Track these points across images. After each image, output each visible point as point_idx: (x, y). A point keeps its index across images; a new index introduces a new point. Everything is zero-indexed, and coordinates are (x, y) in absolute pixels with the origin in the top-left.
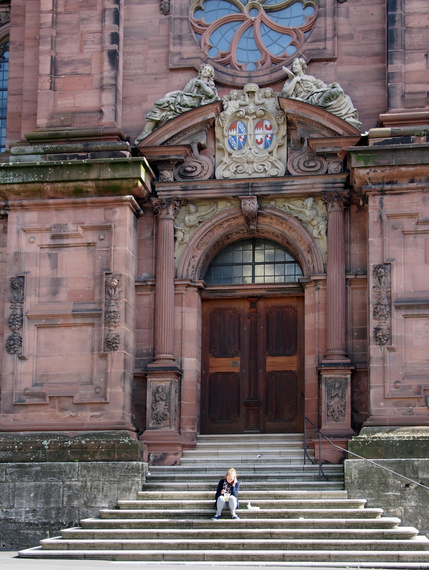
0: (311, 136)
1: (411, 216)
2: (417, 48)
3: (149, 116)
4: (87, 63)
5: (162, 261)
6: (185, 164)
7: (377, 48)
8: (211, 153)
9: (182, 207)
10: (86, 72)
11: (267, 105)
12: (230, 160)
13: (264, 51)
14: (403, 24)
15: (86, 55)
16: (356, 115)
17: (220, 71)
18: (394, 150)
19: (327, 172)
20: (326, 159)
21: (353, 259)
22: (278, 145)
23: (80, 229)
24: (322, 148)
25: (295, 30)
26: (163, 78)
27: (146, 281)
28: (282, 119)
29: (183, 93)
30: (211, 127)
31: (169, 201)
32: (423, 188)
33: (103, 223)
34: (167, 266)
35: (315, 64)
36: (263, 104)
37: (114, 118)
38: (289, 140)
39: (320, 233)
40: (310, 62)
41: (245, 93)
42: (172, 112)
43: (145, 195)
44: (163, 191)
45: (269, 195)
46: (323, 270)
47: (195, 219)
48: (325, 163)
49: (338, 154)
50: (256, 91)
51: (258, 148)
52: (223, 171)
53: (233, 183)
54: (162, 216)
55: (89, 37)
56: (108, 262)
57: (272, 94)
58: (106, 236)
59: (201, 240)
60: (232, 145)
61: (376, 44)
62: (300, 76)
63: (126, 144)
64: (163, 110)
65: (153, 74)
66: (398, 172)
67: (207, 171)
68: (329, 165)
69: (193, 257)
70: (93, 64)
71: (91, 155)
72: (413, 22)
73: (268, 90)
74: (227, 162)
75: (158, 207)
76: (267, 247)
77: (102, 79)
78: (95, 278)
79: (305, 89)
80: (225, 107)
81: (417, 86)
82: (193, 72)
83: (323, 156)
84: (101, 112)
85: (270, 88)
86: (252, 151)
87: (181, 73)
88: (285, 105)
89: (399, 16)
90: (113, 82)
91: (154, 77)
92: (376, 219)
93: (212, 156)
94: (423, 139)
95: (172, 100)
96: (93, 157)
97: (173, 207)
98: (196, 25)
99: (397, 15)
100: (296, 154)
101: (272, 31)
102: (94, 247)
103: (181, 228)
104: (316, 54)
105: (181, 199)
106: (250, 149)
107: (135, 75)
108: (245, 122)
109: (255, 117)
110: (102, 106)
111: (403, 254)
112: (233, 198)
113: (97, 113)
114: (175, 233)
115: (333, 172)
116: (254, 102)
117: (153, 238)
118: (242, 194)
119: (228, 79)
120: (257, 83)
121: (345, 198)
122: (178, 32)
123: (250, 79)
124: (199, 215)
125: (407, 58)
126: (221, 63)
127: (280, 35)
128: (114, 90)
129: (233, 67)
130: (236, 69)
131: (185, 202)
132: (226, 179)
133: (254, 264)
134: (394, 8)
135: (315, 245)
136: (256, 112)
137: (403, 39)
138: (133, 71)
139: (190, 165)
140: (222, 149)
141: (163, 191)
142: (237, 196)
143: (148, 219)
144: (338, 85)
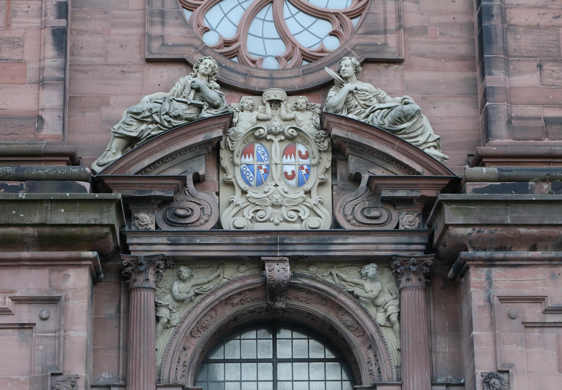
0: (370, 171)
3: (118, 129)
4: (18, 43)
5: (138, 355)
6: (175, 204)
7: (463, 49)
8: (213, 188)
9: (168, 270)
10: (15, 57)
11: (300, 121)
15: (15, 33)
16: (438, 145)
17: (225, 67)
18: (507, 202)
19: (397, 227)
20: (395, 207)
21: (440, 360)
23: (8, 300)
25: (337, 14)
26: (134, 72)
28: (326, 144)
30: (213, 149)
31: (150, 260)
32: (551, 259)
35: (371, 66)
36: (294, 119)
38: (334, 175)
39: (388, 319)
41: (265, 102)
43: (111, 249)
45: (307, 256)
46: (395, 376)
47: (188, 290)
48: (395, 214)
49: (415, 201)
50: (283, 100)
51: (289, 185)
52: (233, 217)
53: (250, 239)
54: (136, 284)
55: (20, 6)
57: (308, 105)
58: (52, 313)
59: (198, 323)
60: (248, 178)
61: (460, 44)
62: (352, 82)
63: (85, 171)
64: (141, 121)
65: (118, 65)
67: (209, 216)
68: (401, 217)
69: (185, 349)
70: (26, 46)
73: (302, 100)
75: (131, 270)
76: (296, 335)
79: (362, 102)
80: (235, 120)
81: (528, 108)
84: (40, 119)
85: (304, 97)
87: (163, 66)
90: (59, 75)
91: (120, 69)
92: (482, 303)
95: (156, 107)
97: (154, 269)
99: (495, 7)
100: (349, 197)
101: (301, 13)
102: (30, 330)
103: (167, 303)
104: (372, 52)
107: (90, 65)
108: (267, 145)
110: (42, 109)
115: (407, 227)
116: (280, 116)
118: (266, 254)
119: (238, 81)
120: (283, 88)
124: (195, 284)
125: (511, 67)
126: (225, 55)
127: (315, 19)
128: (62, 86)
130: (248, 65)
131: (173, 263)
132: (239, 232)
133: (275, 361)
135: (382, 337)
136: (283, 131)
137: (505, 41)
138: (87, 59)
140: (230, 184)
143: (110, 287)
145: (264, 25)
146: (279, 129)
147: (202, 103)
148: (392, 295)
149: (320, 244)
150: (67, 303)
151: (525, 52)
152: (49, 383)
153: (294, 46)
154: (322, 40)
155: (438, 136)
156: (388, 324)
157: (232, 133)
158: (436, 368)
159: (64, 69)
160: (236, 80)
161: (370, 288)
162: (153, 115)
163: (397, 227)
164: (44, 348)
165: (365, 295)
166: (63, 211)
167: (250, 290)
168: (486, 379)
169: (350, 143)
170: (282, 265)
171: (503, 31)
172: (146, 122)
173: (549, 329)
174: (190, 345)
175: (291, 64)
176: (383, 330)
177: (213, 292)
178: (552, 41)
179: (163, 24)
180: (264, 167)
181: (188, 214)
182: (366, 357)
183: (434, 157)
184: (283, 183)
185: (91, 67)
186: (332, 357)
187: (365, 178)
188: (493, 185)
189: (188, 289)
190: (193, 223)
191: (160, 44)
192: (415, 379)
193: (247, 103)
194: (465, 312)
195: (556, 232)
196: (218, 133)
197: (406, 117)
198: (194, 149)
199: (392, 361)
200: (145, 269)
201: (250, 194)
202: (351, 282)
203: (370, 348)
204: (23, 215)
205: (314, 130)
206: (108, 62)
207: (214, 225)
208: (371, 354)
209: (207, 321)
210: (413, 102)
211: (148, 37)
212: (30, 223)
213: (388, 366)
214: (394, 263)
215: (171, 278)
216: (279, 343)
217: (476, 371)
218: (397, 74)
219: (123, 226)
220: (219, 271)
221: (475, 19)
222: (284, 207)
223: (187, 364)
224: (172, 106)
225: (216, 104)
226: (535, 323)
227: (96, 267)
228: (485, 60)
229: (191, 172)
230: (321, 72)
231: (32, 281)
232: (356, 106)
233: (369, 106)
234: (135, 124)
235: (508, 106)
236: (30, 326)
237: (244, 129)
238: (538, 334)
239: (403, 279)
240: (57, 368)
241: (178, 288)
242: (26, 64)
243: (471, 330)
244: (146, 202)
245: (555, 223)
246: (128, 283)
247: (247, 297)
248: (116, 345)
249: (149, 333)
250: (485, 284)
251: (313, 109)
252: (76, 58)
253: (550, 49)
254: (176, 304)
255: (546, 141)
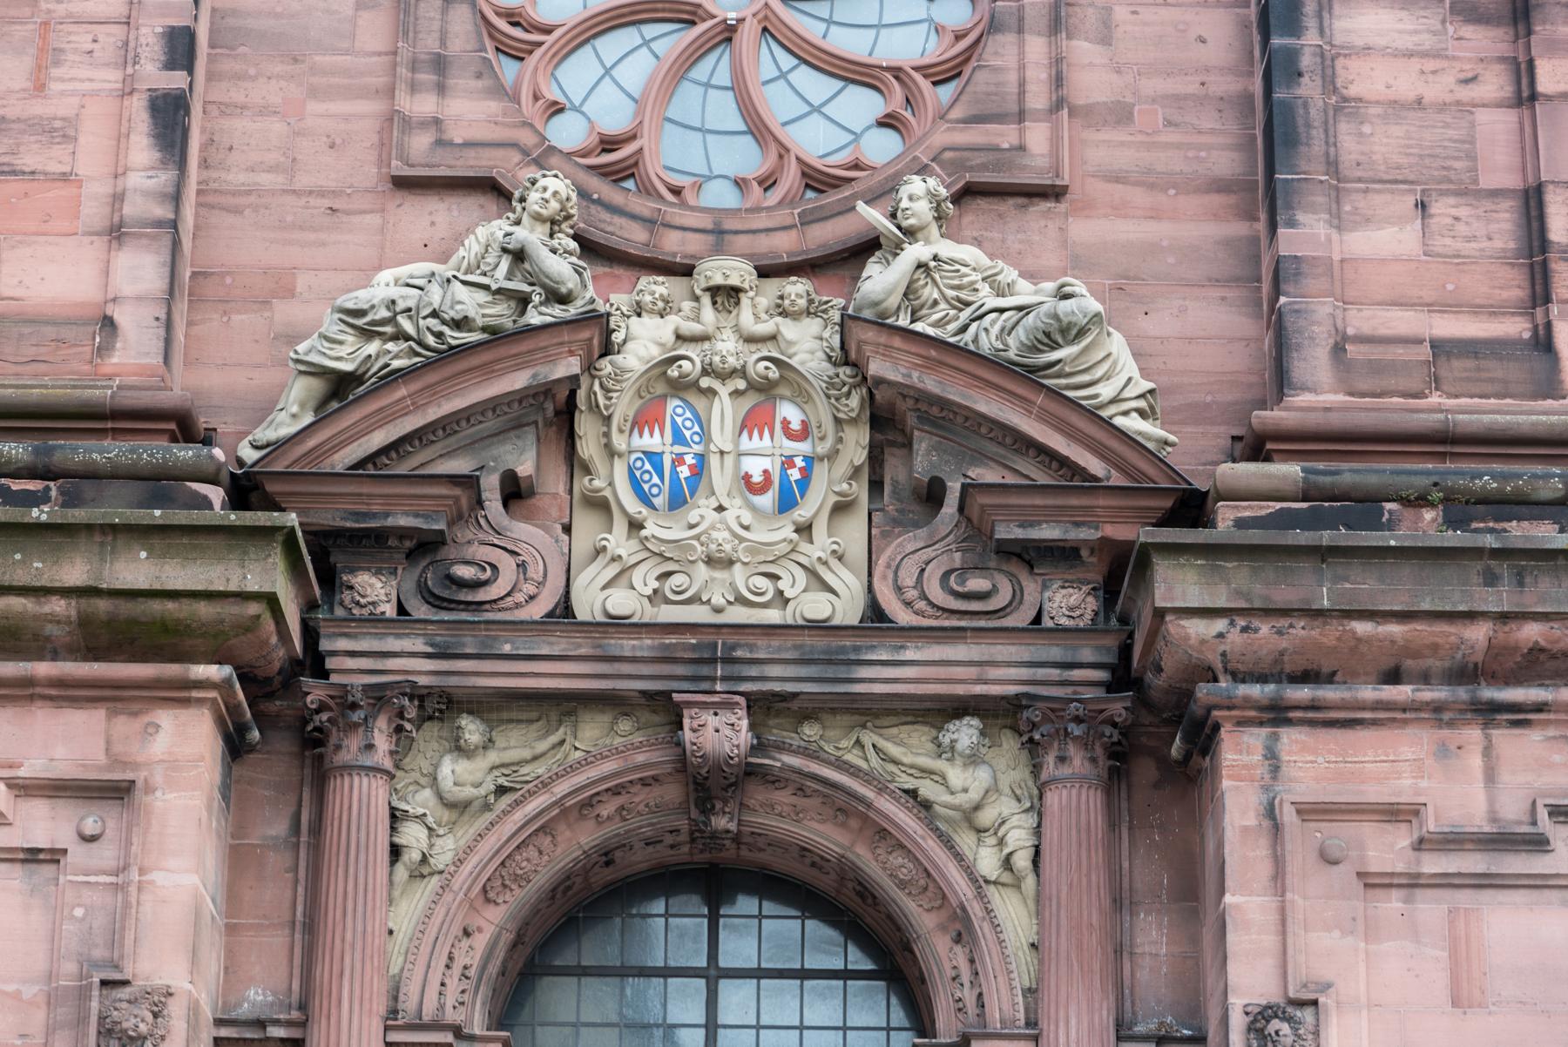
0: (970, 473)
1: (1395, 813)
2: (1386, 177)
3: (306, 354)
4: (61, 132)
6: (449, 552)
7: (1225, 162)
8: (554, 512)
9: (427, 724)
11: (790, 343)
12: (634, 545)
13: (776, 139)
14: (1330, 83)
15: (56, 106)
16: (1152, 407)
17: (599, 202)
19: (1037, 620)
20: (1032, 567)
21: (1143, 975)
22: (834, 499)
24: (1021, 526)
25: (897, 72)
27: (261, 1024)
28: (854, 401)
29: (449, 274)
30: (557, 413)
31: (379, 696)
32: (1437, 708)
33: (100, 769)
34: (358, 965)
35: (982, 203)
37: (162, 351)
38: (876, 486)
39: (1007, 864)
40: (967, 194)
41: (698, 292)
42: (404, 345)
43: (277, 665)
44: (352, 654)
45: (795, 695)
46: (1021, 1016)
48: (1031, 587)
49: (1084, 553)
51: (753, 509)
52: (604, 588)
53: (644, 645)
54: (344, 757)
55: (72, 38)
56: (115, 936)
57: (811, 302)
58: (111, 824)
59: (503, 863)
60: (646, 487)
61: (1220, 151)
62: (927, 242)
63: (212, 457)
64: (367, 334)
65: (322, 193)
66: (1339, 639)
67: (541, 584)
68: (1047, 594)
69: (467, 933)
70: (82, 140)
71: (62, 492)
72: (1366, 80)
73: (797, 288)
74: (622, 552)
75: (329, 720)
76: (769, 907)
77: (118, 198)
78: (52, 999)
79: (951, 293)
80: (618, 337)
81: (1389, 314)
82: (489, 196)
83: (1019, 556)
84: (108, 323)
86: (723, 516)
88: (868, 350)
89: (1314, 55)
90: (163, 212)
91: (327, 203)
92: (1251, 820)
93: (559, 528)
94: (1428, 515)
95: (409, 298)
96: (70, 500)
97: (390, 721)
98: (502, 24)
99: (1307, 50)
100: (910, 541)
101: (804, 67)
102: (53, 867)
103: (421, 811)
104: (984, 167)
105: (425, 691)
106: (720, 509)
107: (249, 193)
108: (700, 403)
109: (741, 384)
110: (114, 300)
111: (1362, 968)
112: (643, 701)
113: (90, 329)
114: (393, 829)
115: (1064, 621)
117: (297, 846)
119: (632, 236)
121: (1115, 725)
122: (430, 43)
123: (720, 236)
124: (498, 762)
125: (1347, 208)
126: (603, 171)
127: (841, 84)
128: (166, 241)
129: (647, 190)
130: (661, 197)
131: (440, 706)
132: (617, 624)
133: (713, 974)
134: (1294, 27)
135: (989, 911)
137: (1332, 140)
139: (469, 557)
140: (601, 505)
141: (352, 654)
142: (667, 695)
143: (276, 763)
144: (1079, 287)
145: (708, 100)
146: (732, 361)
147: (527, 289)
148: (1019, 800)
149: (830, 662)
150: (148, 799)
151: (1382, 168)
152: (95, 1005)
153: (784, 151)
154: (857, 137)
155: (1150, 385)
156: (1006, 878)
157: (609, 369)
158: (1132, 994)
159: (176, 198)
160: (626, 236)
161: (963, 782)
162: (399, 318)
163: (1037, 620)
164: (85, 915)
165: (947, 798)
166: (143, 554)
167: (644, 782)
168: (1255, 1021)
169: (917, 400)
170: (726, 717)
171: (1325, 111)
172: (380, 334)
173: (1429, 892)
174: (483, 923)
175: (774, 197)
176: (991, 891)
177: (545, 785)
178: (1455, 141)
179: (441, 89)
180: (689, 460)
181: (484, 577)
182: (947, 966)
183: (1139, 438)
184: (738, 502)
185: (252, 199)
186: (868, 965)
187: (954, 487)
188: (1289, 509)
189: (479, 776)
190: (495, 601)
191: (432, 140)
192: (1073, 1022)
193: (652, 293)
194: (1211, 847)
195: (1451, 634)
196: (569, 366)
197: (1064, 331)
198: (506, 409)
199: (1015, 975)
200: (366, 719)
201: (650, 529)
202: (912, 767)
203: (958, 939)
204: (40, 565)
205: (826, 365)
206: (297, 186)
207: (550, 606)
208: (960, 957)
209: (528, 860)
210: (1084, 292)
211: (395, 123)
212: (57, 584)
213: (1004, 991)
214: (1025, 714)
215: (435, 745)
216: (725, 926)
217: (1231, 999)
218: (1050, 223)
219: (310, 606)
220: (562, 730)
221: (1257, 86)
222: (738, 566)
223: (472, 972)
224: (449, 294)
225: (564, 290)
226: (1392, 874)
227: (233, 709)
228: (1279, 187)
229: (494, 469)
230: (850, 216)
231: (65, 740)
232: (936, 303)
233: (968, 304)
234: (350, 339)
235: (1336, 307)
236: (53, 856)
237: (640, 359)
238: (1400, 905)
239: (1050, 760)
240: (116, 967)
241: (451, 770)
242: (79, 183)
243: (1222, 891)
244: (371, 543)
245: (1448, 608)
246: (321, 757)
247: (637, 800)
248: (287, 916)
249: (370, 887)
250: (1262, 770)
251: (825, 311)
252: (215, 175)
253: (1448, 163)
254: (446, 815)
255: (1435, 399)
